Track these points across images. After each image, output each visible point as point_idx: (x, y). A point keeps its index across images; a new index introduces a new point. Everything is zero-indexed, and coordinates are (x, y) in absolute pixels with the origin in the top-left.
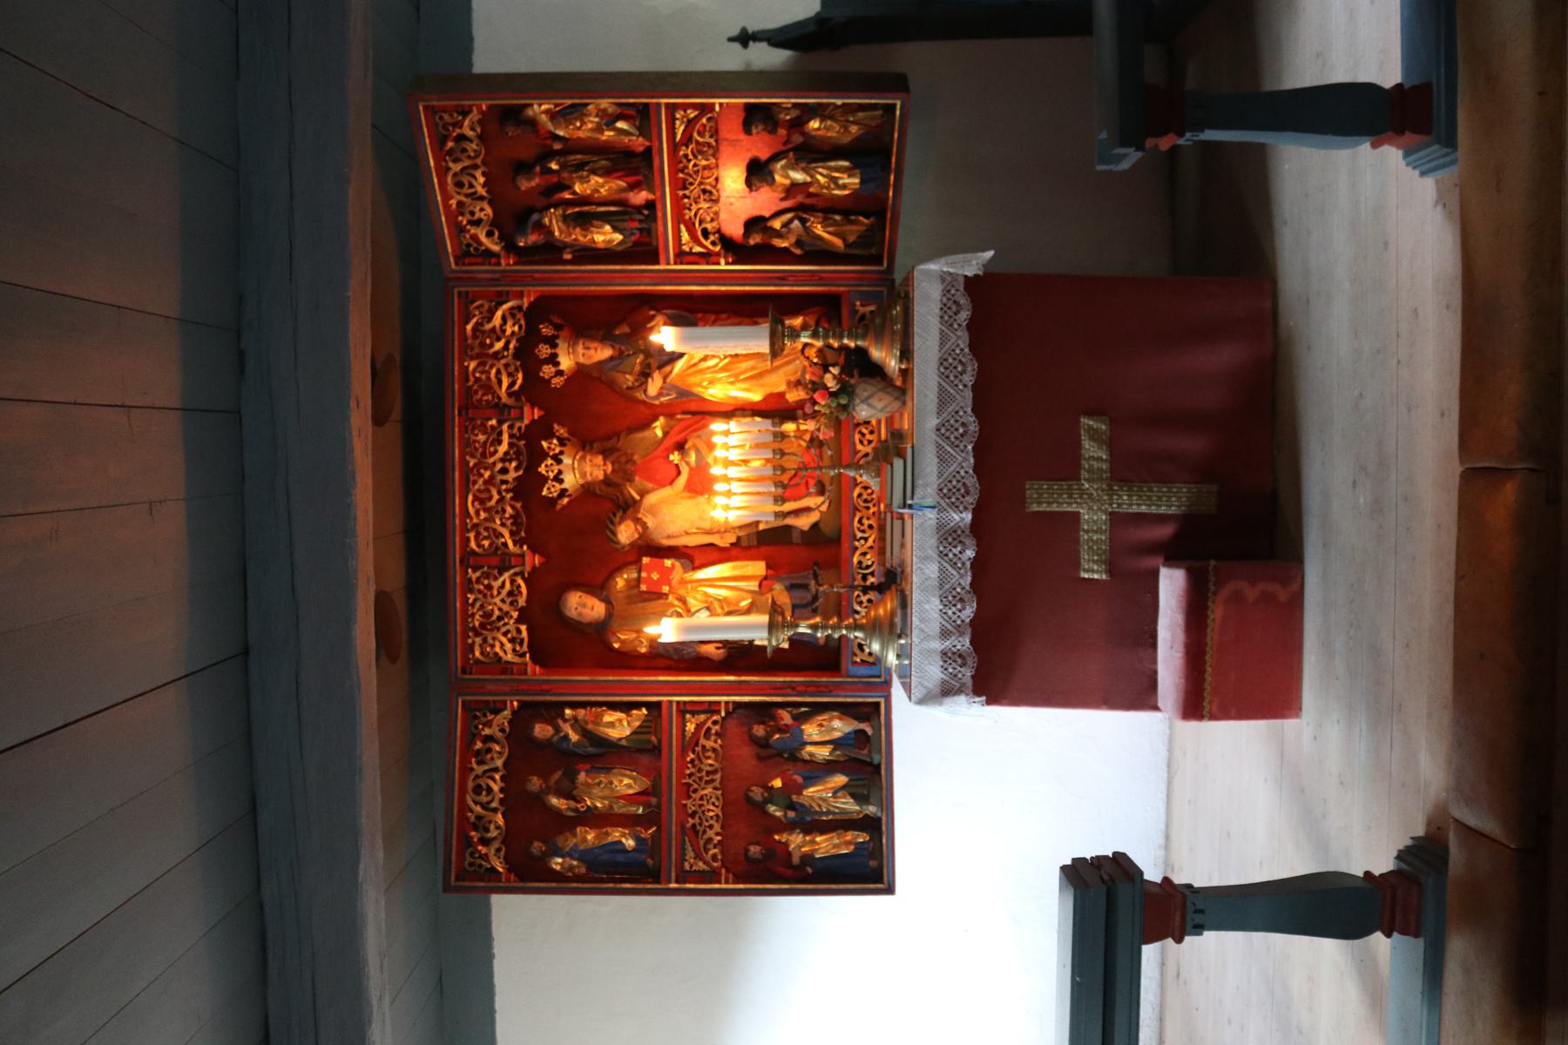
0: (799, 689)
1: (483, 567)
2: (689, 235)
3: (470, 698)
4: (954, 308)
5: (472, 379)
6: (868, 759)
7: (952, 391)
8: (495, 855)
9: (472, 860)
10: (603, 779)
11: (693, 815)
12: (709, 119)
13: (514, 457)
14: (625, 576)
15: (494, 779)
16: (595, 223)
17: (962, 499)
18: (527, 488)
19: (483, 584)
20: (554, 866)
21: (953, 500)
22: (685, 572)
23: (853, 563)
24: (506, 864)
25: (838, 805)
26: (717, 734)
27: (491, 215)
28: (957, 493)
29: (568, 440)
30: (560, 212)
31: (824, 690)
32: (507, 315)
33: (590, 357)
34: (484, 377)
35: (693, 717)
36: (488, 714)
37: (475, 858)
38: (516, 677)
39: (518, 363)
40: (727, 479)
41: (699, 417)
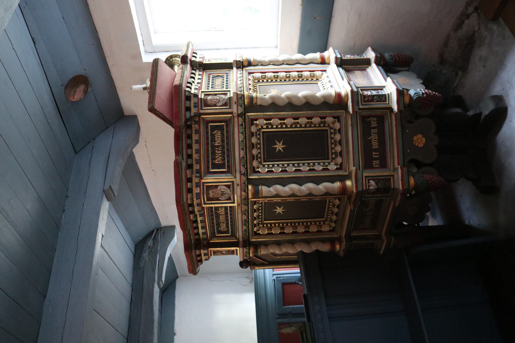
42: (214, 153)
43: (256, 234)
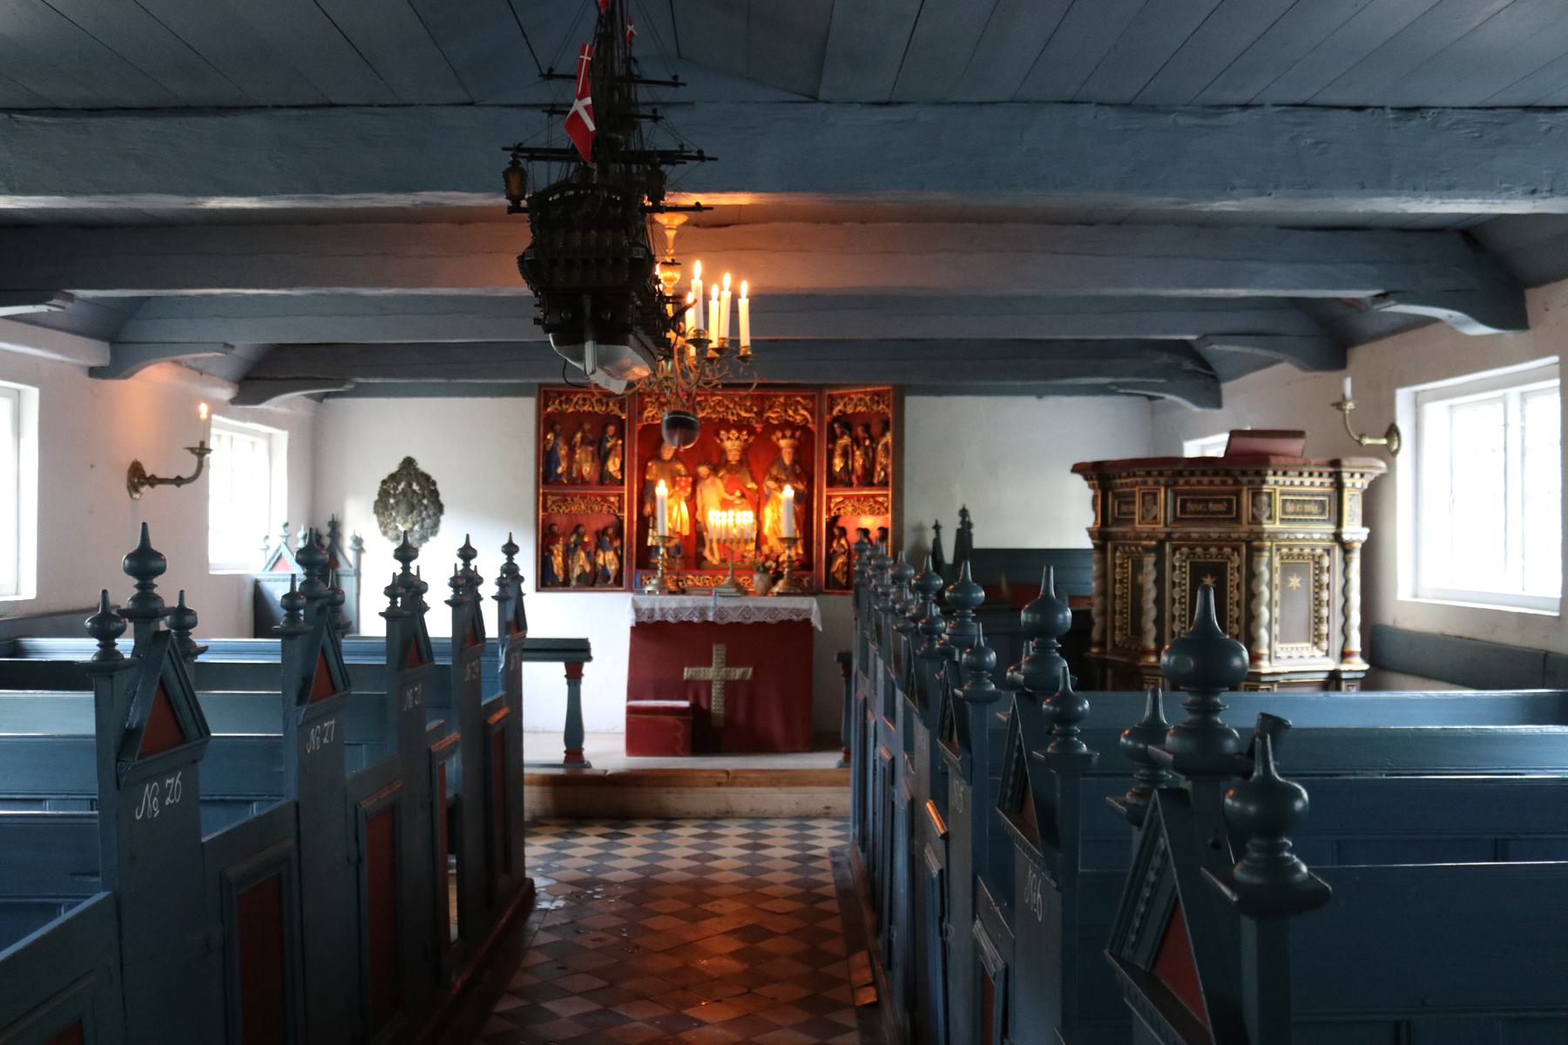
11: (572, 500)
18: (725, 425)
42: (1199, 501)
43: (1115, 549)
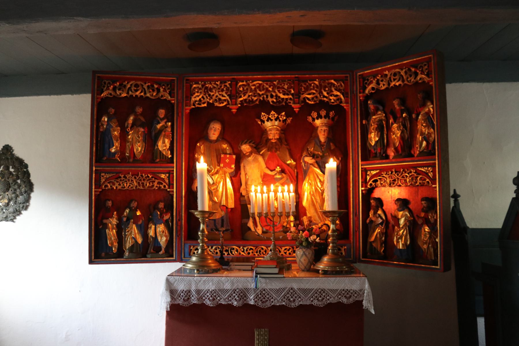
0: (179, 222)
1: (231, 88)
2: (375, 174)
3: (176, 82)
4: (348, 296)
5: (311, 82)
6: (148, 253)
7: (310, 295)
8: (109, 93)
9: (107, 83)
10: (141, 138)
11: (125, 177)
12: (428, 182)
13: (278, 100)
14: (228, 148)
15: (141, 92)
16: (379, 133)
17: (260, 300)
19: (224, 88)
20: (103, 118)
21: (260, 296)
22: (229, 174)
23: (233, 246)
24: (105, 98)
25: (129, 239)
26: (160, 187)
27: (382, 89)
28: (263, 298)
29: (285, 124)
30: (383, 118)
31: (178, 234)
32: (338, 97)
33: (320, 132)
34: (312, 87)
35: (167, 177)
36: (169, 90)
37: (108, 84)
38: (184, 102)
39: (318, 102)
40: (269, 191)
41: (295, 178)
